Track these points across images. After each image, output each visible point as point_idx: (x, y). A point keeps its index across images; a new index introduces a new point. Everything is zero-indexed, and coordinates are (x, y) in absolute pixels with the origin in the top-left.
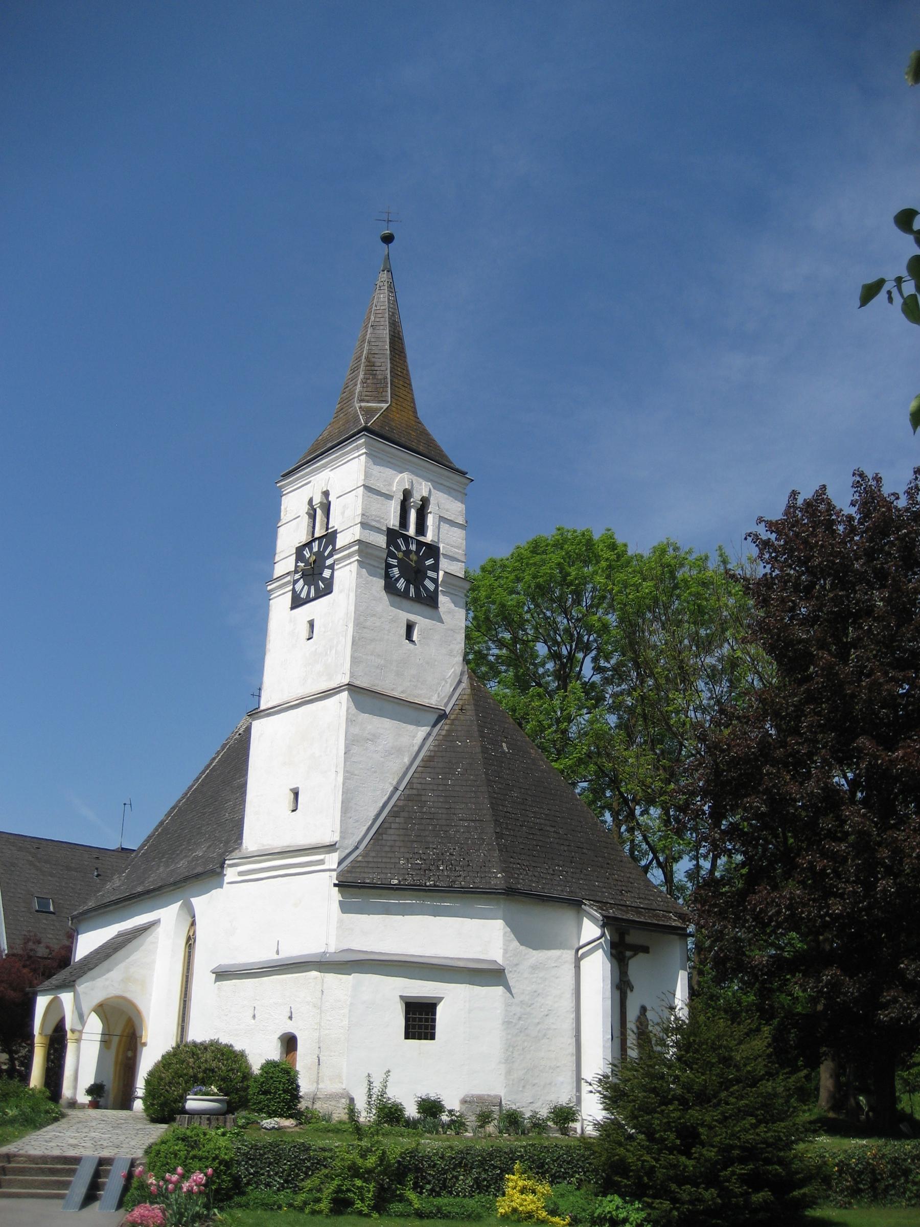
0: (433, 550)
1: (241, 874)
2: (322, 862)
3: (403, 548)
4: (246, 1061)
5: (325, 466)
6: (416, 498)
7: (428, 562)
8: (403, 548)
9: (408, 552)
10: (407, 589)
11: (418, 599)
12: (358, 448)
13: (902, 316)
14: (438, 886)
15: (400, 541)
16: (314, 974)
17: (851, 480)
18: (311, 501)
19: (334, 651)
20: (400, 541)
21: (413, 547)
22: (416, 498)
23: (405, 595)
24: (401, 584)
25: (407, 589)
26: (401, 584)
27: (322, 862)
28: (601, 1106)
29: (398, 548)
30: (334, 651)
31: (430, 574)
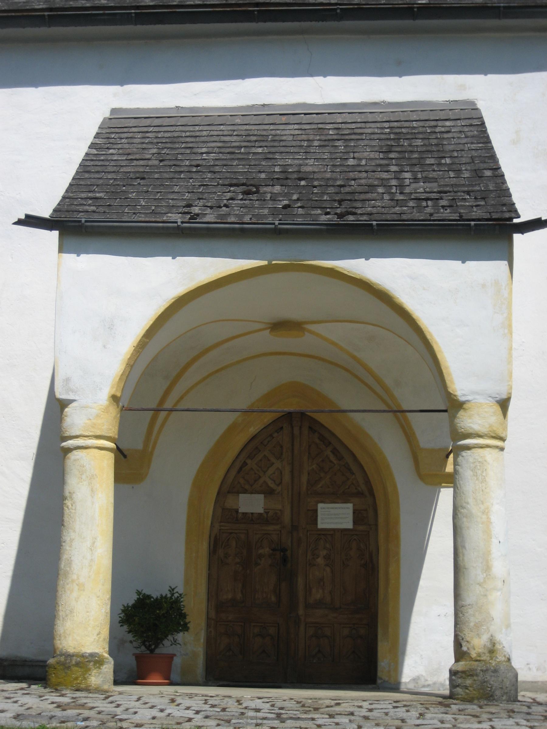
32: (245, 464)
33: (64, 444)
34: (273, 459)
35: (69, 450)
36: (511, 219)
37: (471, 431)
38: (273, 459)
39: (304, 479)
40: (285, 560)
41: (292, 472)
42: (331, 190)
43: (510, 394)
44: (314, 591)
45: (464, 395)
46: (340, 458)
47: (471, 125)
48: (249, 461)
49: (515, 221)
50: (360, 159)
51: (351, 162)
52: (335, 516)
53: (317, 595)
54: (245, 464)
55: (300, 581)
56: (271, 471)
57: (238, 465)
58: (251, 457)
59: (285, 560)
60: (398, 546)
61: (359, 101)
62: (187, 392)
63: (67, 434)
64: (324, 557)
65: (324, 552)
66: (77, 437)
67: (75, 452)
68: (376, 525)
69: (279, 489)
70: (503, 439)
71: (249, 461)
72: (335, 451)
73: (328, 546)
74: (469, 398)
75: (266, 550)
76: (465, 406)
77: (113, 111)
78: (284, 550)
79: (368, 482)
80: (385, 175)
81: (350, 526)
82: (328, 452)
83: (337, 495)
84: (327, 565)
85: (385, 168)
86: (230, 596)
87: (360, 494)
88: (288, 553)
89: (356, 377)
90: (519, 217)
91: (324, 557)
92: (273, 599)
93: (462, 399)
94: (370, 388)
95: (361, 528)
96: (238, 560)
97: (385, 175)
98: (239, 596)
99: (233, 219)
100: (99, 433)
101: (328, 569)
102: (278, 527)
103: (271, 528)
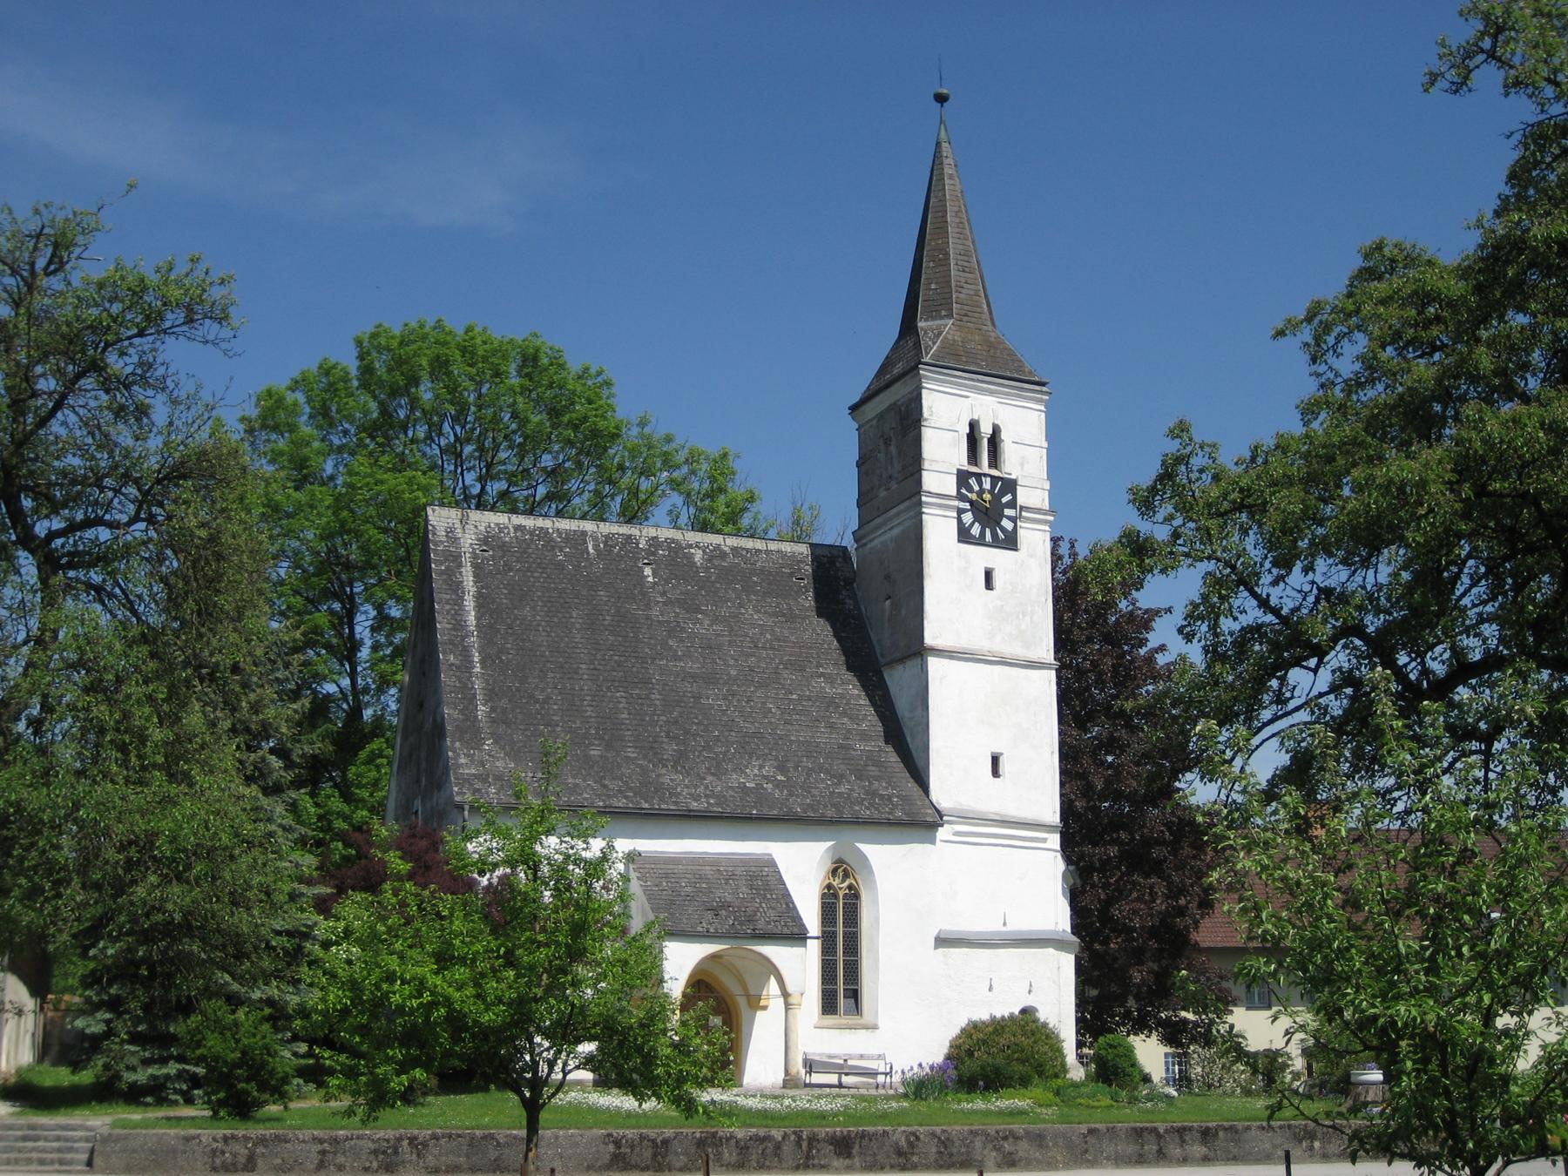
0: (1010, 486)
1: (957, 834)
2: (1044, 840)
3: (976, 488)
4: (958, 1037)
5: (991, 393)
6: (986, 430)
7: (1004, 500)
8: (976, 488)
9: (982, 491)
10: (983, 534)
11: (996, 544)
12: (1039, 401)
13: (963, 1023)
14: (908, 509)
15: (973, 481)
16: (1051, 950)
17: (1172, 574)
18: (973, 426)
19: (1028, 619)
20: (973, 481)
21: (987, 484)
22: (986, 430)
23: (980, 541)
24: (976, 530)
25: (983, 534)
26: (976, 530)
27: (1044, 840)
28: (333, 361)
29: (970, 490)
30: (1028, 619)
31: (1008, 512)
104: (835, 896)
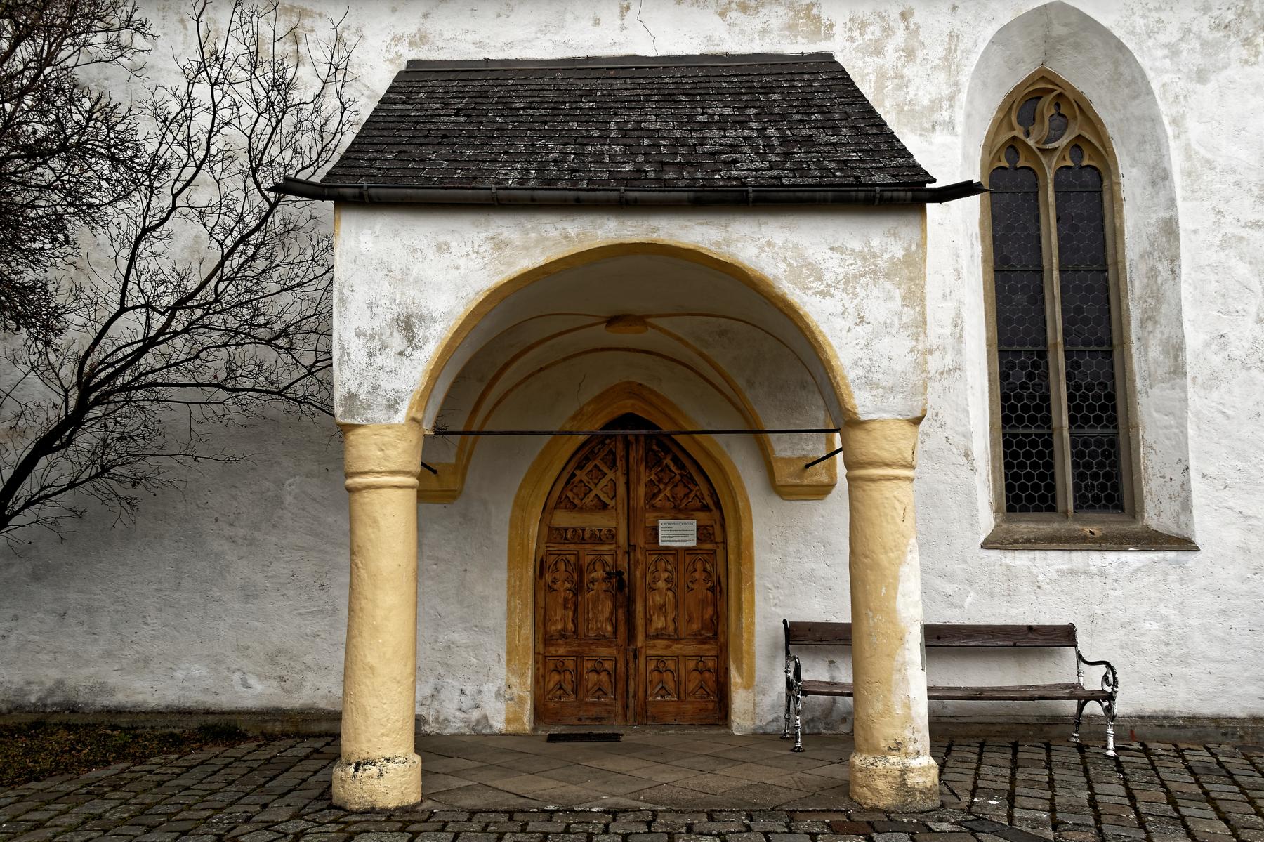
32: (573, 475)
33: (349, 482)
34: (605, 469)
35: (350, 490)
36: (924, 184)
37: (876, 458)
38: (605, 469)
39: (642, 491)
40: (621, 586)
41: (627, 483)
42: (682, 151)
43: (925, 410)
44: (655, 618)
45: (867, 413)
46: (681, 466)
47: (833, 79)
48: (578, 472)
49: (928, 186)
50: (711, 116)
51: (702, 119)
52: (678, 534)
53: (659, 623)
54: (573, 475)
55: (639, 608)
56: (604, 482)
57: (565, 476)
58: (580, 466)
59: (621, 586)
60: (752, 569)
61: (698, 53)
62: (506, 395)
63: (353, 469)
64: (666, 580)
65: (666, 575)
66: (366, 473)
67: (365, 494)
68: (725, 542)
69: (612, 503)
70: (913, 467)
71: (578, 472)
72: (676, 460)
73: (669, 567)
74: (874, 417)
75: (599, 574)
76: (867, 427)
77: (410, 63)
78: (620, 574)
79: (714, 494)
80: (746, 133)
81: (693, 543)
82: (668, 461)
83: (679, 512)
84: (669, 589)
85: (743, 125)
86: (559, 627)
87: (705, 508)
88: (625, 576)
89: (701, 375)
90: (934, 181)
91: (666, 580)
92: (609, 628)
93: (863, 418)
94: (729, 400)
95: (708, 546)
96: (568, 585)
97: (746, 133)
98: (570, 626)
99: (564, 184)
100: (394, 467)
101: (670, 594)
102: (612, 547)
103: (606, 547)
104: (1033, 174)
